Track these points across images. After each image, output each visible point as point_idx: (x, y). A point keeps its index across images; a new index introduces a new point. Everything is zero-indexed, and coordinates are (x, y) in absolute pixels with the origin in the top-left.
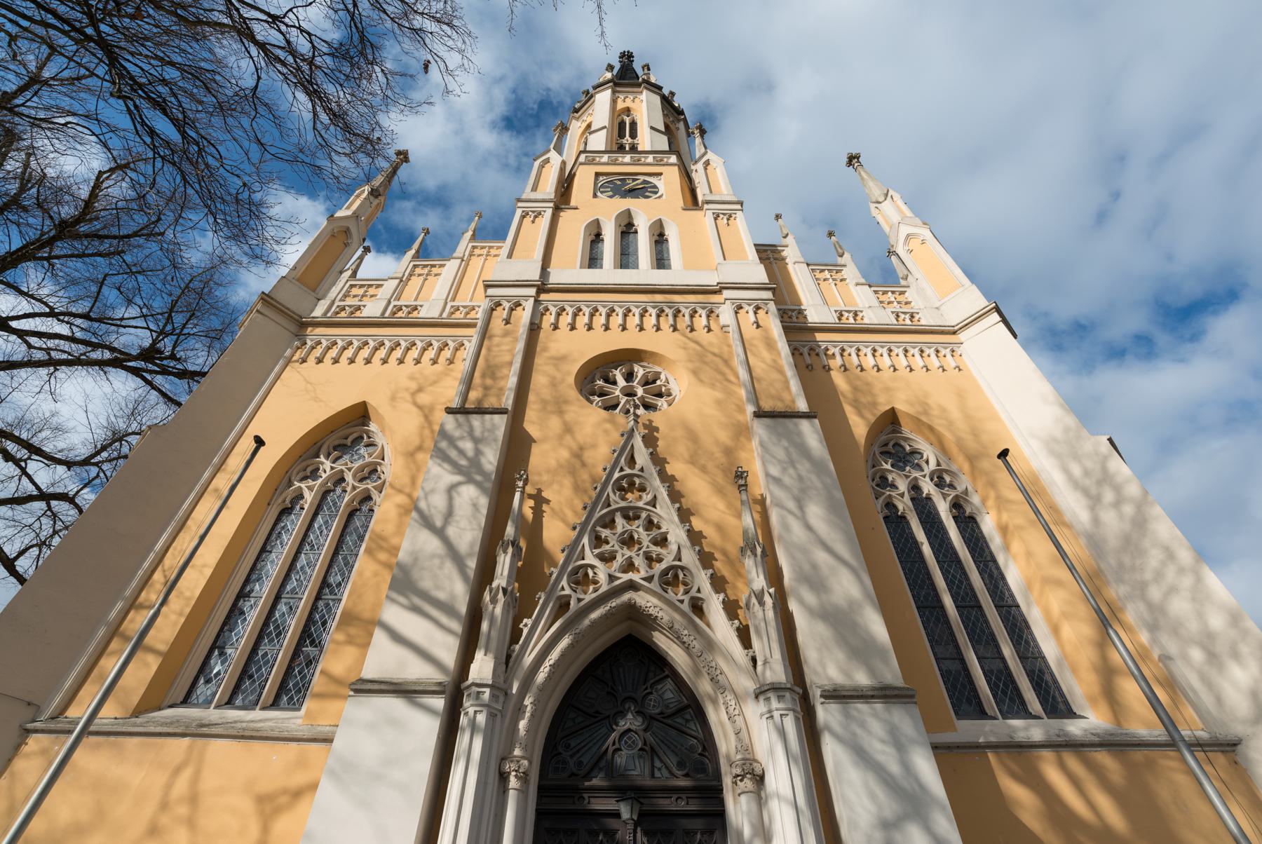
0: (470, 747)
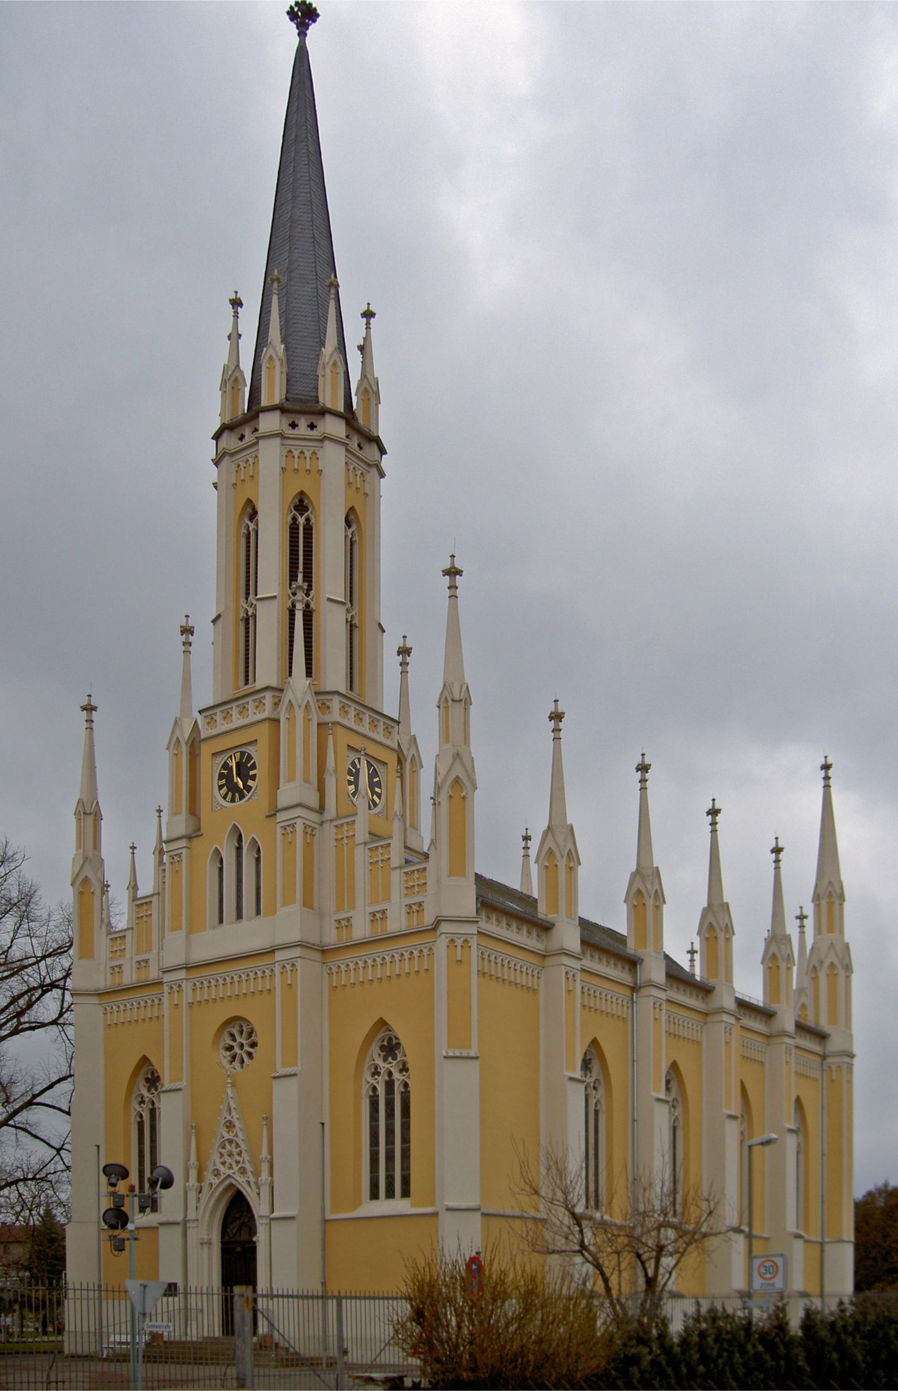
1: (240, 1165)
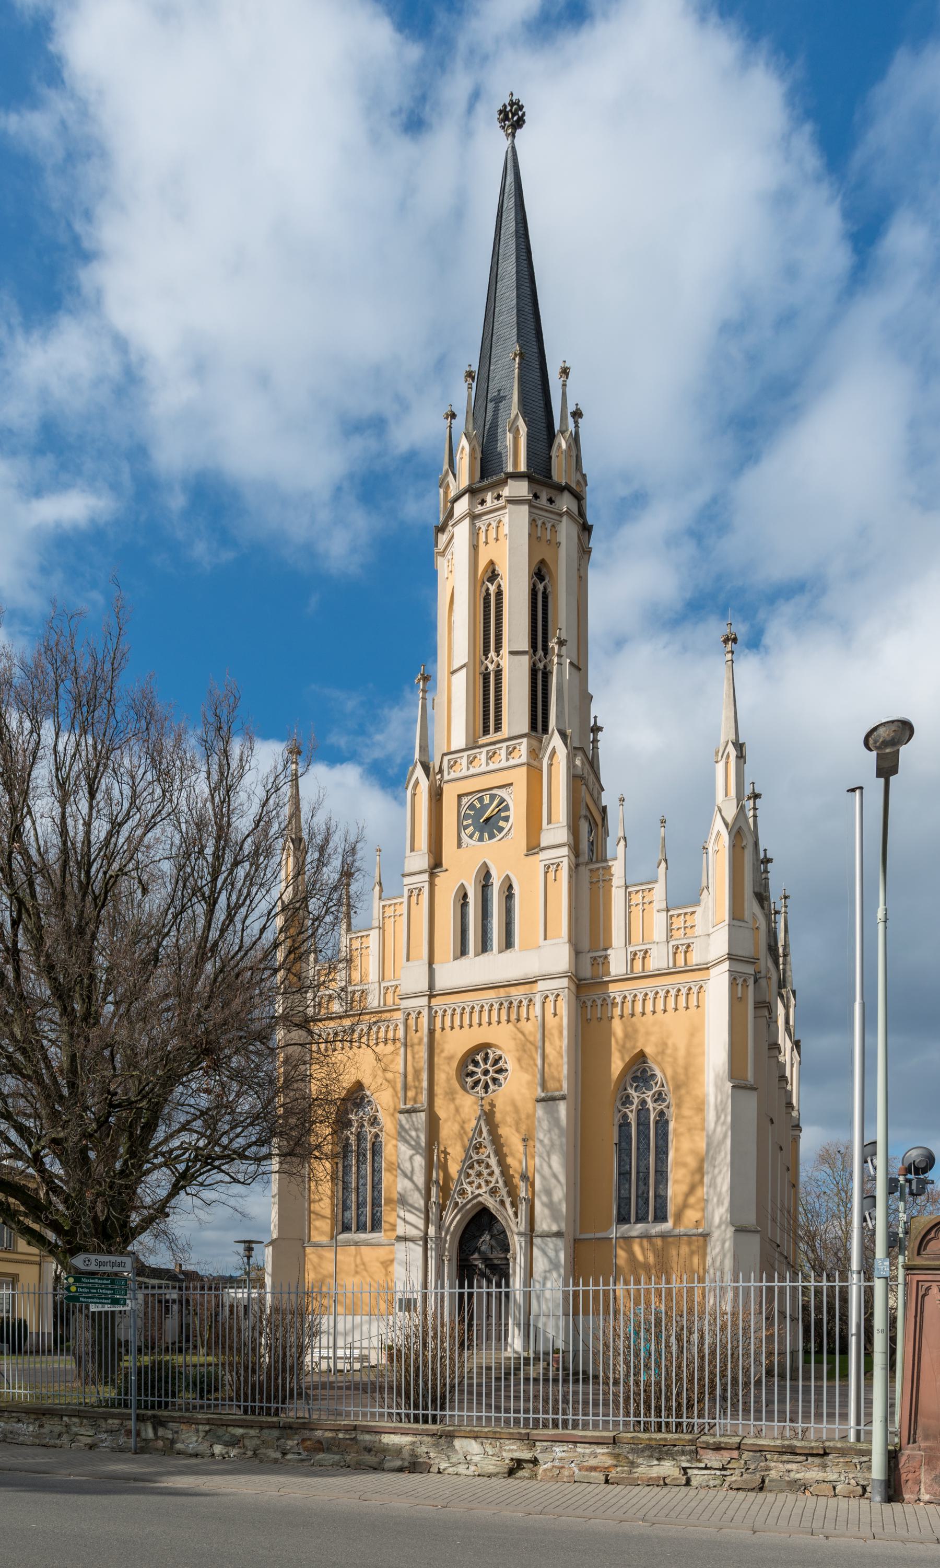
0: (432, 1254)
1: (492, 1185)
